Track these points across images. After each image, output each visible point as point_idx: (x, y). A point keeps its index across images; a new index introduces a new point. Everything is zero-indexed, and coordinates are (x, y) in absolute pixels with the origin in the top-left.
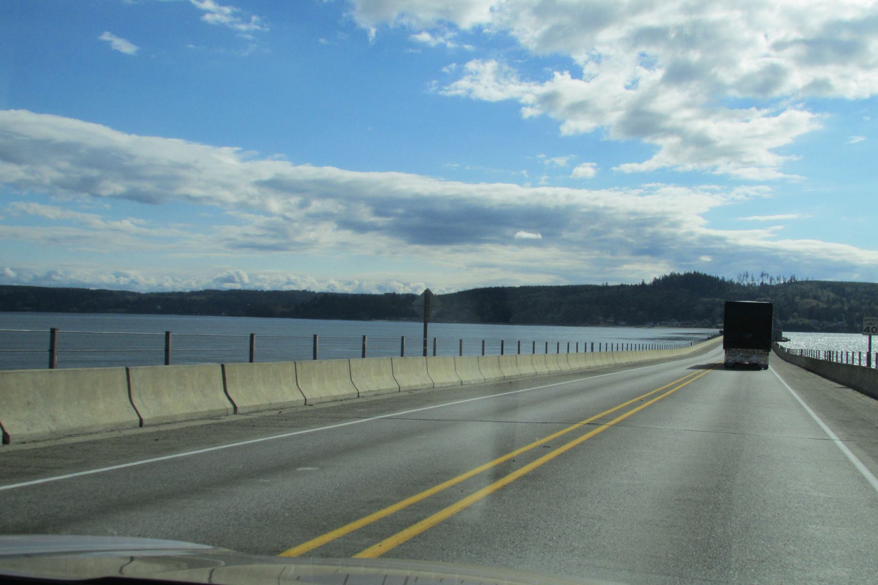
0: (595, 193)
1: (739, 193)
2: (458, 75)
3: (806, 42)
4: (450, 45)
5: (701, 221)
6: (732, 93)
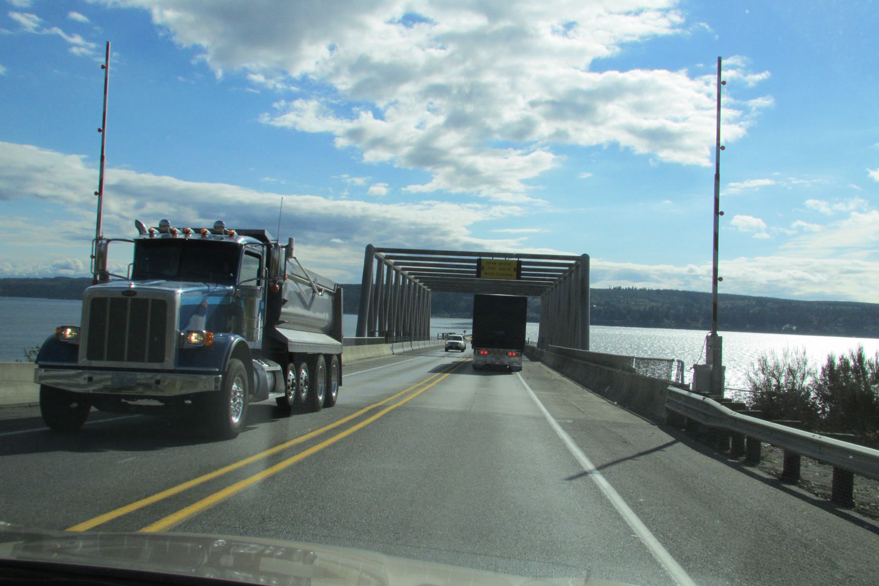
0: (384, 208)
1: (496, 211)
2: (285, 111)
3: (553, 103)
4: (279, 86)
5: (467, 232)
6: (498, 137)
